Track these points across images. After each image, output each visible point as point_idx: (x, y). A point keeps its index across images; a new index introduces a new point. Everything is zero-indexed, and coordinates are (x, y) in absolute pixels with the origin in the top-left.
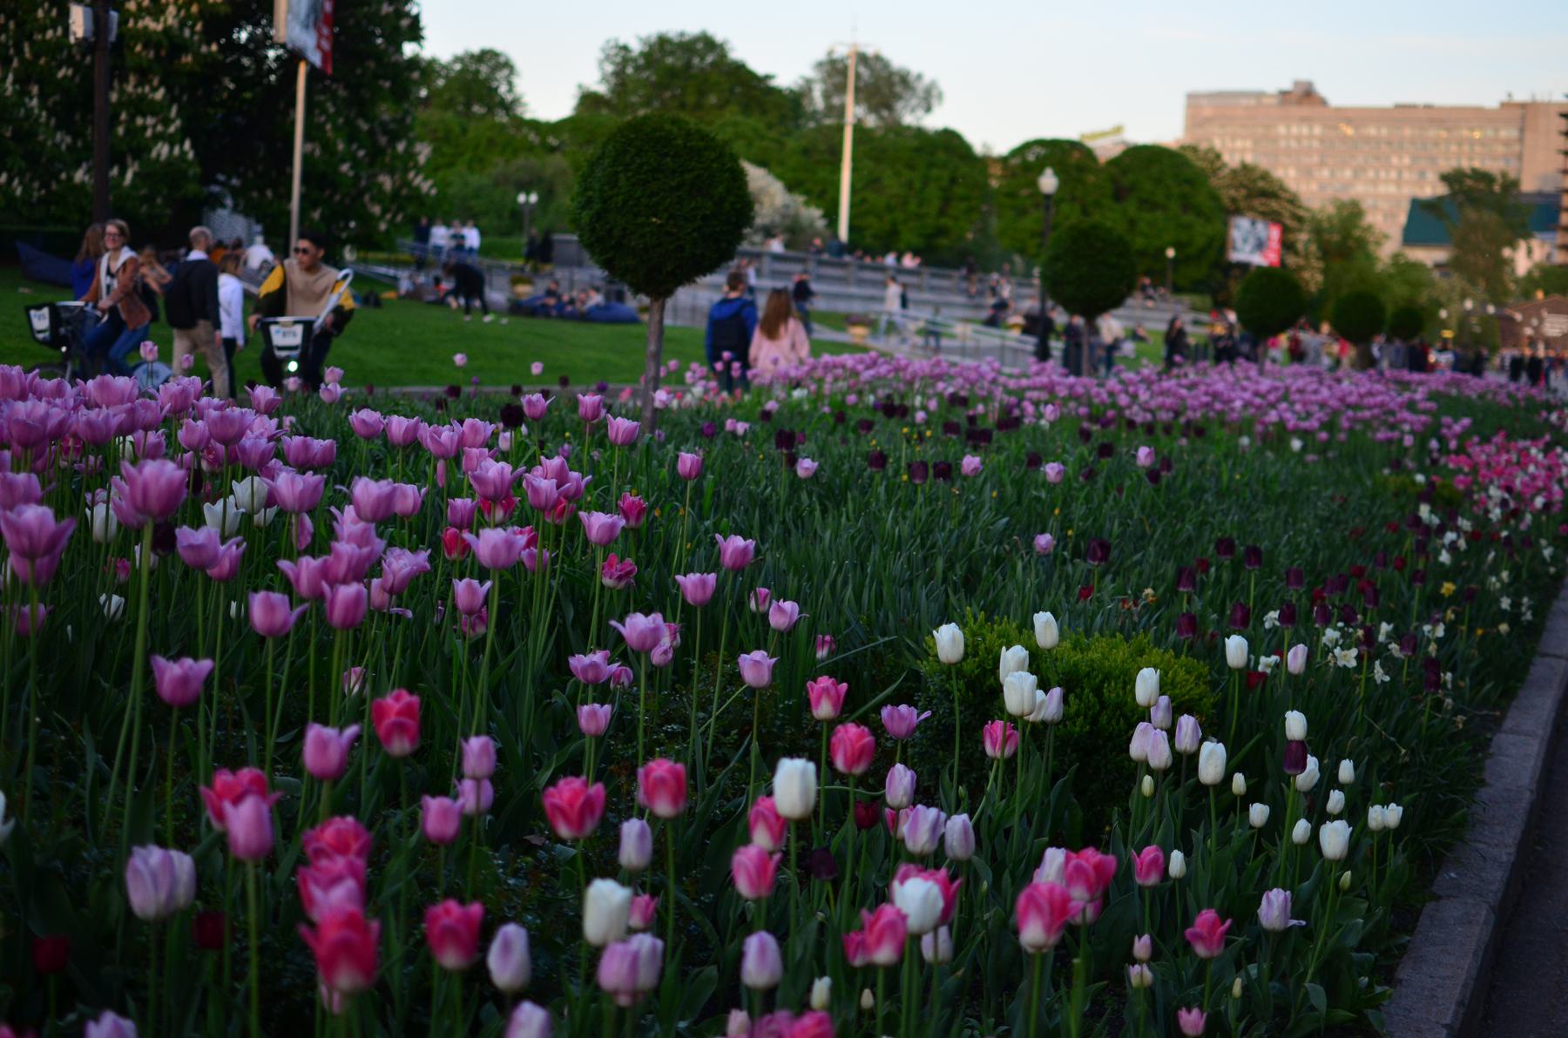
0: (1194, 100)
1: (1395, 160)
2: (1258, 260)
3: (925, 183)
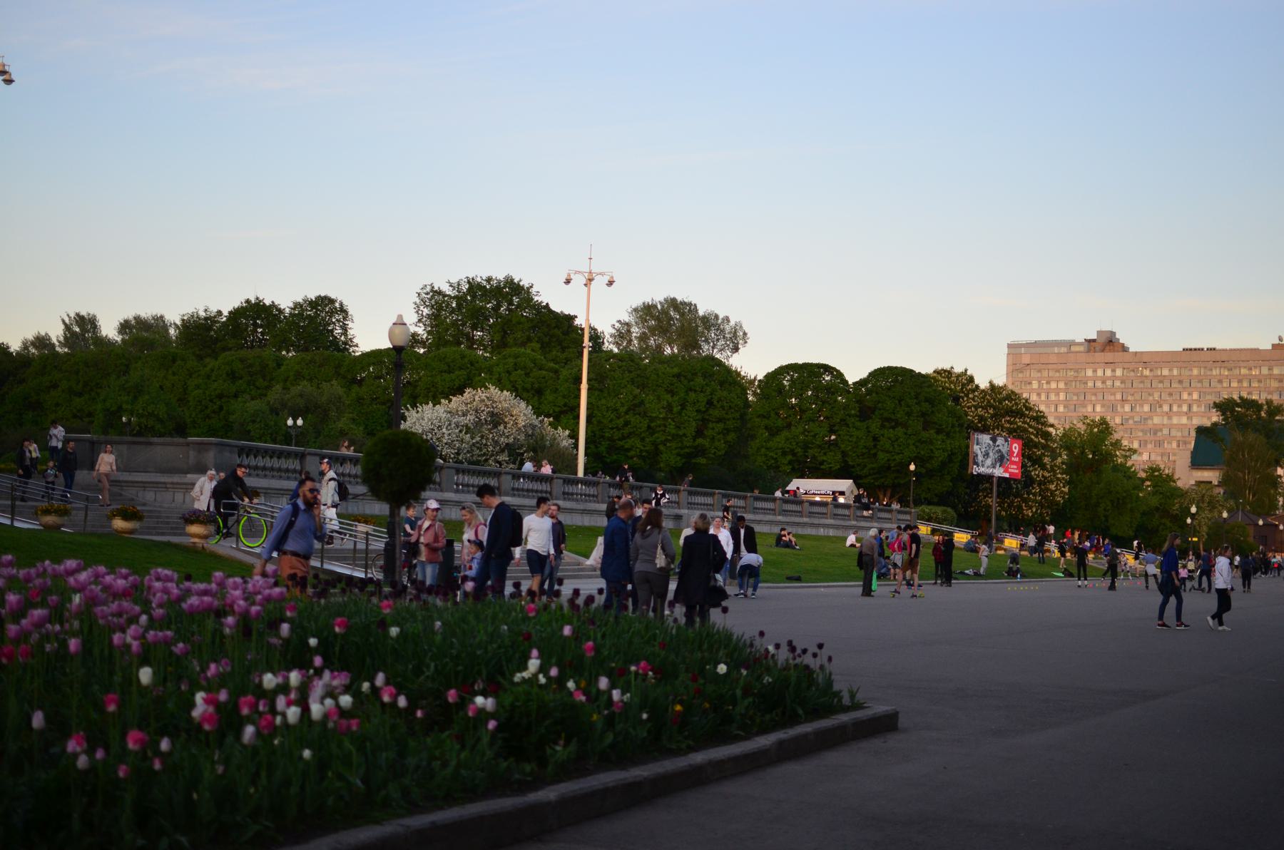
0: (1009, 346)
1: (1185, 396)
2: (999, 472)
3: (683, 406)
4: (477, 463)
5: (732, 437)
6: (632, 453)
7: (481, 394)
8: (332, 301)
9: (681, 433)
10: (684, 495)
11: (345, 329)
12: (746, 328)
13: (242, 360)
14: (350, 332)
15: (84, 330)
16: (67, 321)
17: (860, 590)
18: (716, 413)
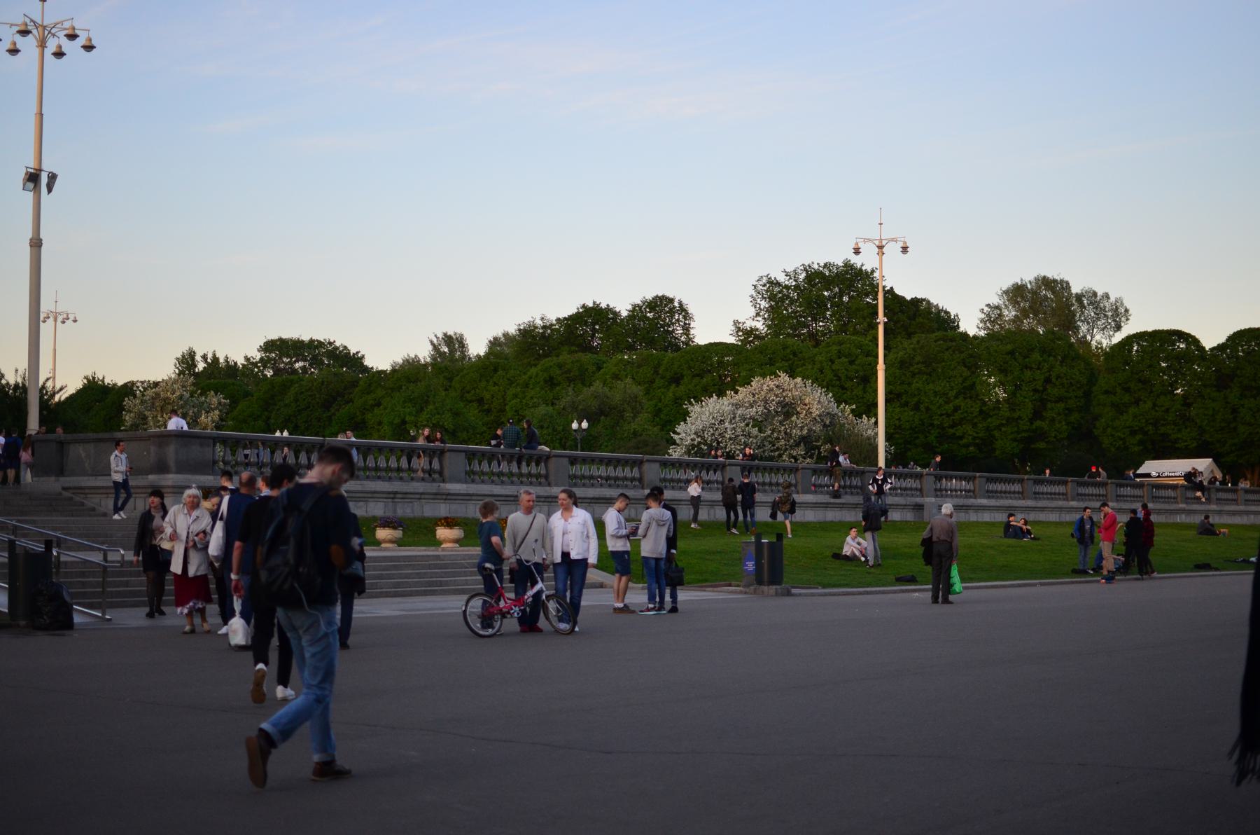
4: (771, 459)
5: (1075, 417)
6: (965, 441)
7: (770, 382)
8: (671, 301)
9: (1016, 415)
10: (929, 483)
11: (687, 329)
12: (1127, 304)
13: (560, 366)
14: (692, 332)
15: (452, 351)
16: (435, 341)
17: (929, 594)
18: (1054, 391)
